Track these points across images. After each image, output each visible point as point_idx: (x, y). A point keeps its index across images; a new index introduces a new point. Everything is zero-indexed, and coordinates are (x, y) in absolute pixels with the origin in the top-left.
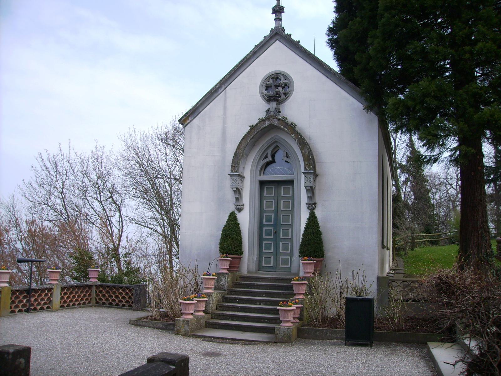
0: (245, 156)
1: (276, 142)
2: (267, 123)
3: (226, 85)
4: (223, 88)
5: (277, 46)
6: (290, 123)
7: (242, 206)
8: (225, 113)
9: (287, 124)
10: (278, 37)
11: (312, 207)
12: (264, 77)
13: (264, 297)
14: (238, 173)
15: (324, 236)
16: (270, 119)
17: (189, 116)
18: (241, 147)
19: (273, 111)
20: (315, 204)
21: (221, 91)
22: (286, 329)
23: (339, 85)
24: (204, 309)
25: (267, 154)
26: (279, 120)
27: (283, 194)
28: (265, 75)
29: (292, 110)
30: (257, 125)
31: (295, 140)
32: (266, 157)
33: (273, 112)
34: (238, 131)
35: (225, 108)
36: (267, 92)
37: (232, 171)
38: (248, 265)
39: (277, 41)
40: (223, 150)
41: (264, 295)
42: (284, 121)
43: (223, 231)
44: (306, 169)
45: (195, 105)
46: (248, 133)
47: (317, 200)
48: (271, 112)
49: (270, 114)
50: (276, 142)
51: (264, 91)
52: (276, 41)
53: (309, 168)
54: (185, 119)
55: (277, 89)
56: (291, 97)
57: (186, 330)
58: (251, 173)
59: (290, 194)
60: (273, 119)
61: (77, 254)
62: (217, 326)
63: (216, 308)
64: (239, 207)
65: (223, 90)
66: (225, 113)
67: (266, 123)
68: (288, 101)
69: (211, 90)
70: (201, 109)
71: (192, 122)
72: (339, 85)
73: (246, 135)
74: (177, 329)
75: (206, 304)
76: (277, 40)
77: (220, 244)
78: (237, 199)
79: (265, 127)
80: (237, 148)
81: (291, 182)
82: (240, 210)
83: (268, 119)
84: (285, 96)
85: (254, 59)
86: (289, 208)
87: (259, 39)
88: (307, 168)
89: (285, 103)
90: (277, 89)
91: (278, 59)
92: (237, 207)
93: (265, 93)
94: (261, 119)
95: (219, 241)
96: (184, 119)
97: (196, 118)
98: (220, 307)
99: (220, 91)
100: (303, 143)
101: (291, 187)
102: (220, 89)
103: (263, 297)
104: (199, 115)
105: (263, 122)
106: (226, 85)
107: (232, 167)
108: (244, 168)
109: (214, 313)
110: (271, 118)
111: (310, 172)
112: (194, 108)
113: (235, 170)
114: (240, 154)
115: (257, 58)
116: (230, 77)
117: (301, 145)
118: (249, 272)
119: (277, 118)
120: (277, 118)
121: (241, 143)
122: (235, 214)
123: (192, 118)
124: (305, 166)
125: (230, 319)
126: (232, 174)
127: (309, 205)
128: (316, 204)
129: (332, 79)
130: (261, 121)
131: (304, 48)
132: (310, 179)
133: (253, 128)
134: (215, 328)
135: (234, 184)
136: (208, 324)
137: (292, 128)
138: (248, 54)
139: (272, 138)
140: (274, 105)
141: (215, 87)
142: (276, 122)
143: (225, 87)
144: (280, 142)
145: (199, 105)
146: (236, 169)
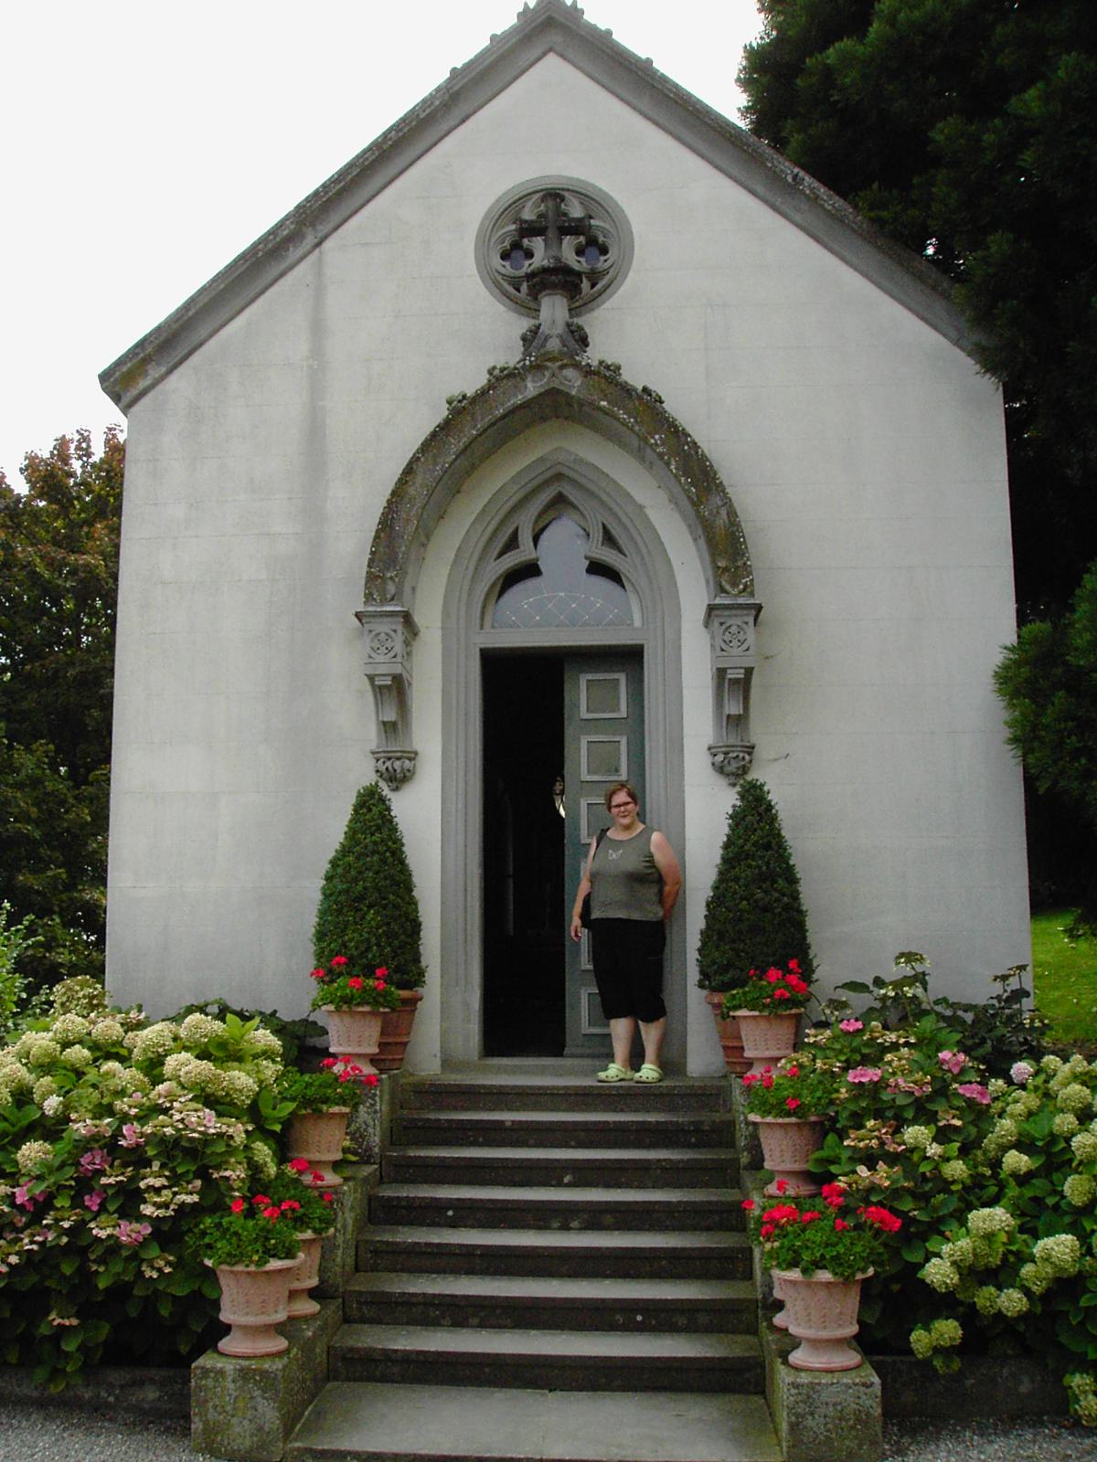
0: (423, 539)
1: (559, 477)
2: (532, 388)
3: (319, 227)
4: (310, 240)
5: (553, 74)
6: (641, 388)
7: (410, 759)
8: (317, 352)
9: (627, 390)
10: (556, 38)
11: (734, 762)
12: (505, 194)
13: (569, 1185)
14: (399, 609)
15: (809, 895)
16: (547, 368)
17: (147, 360)
18: (412, 491)
19: (560, 336)
20: (750, 749)
21: (300, 252)
22: (848, 1386)
23: (835, 247)
24: (314, 1282)
25: (517, 529)
26: (588, 372)
27: (588, 710)
28: (492, 200)
29: (635, 333)
30: (483, 394)
31: (668, 464)
32: (512, 543)
33: (557, 341)
34: (385, 428)
35: (318, 329)
36: (507, 264)
37: (369, 597)
38: (444, 1034)
39: (551, 54)
40: (313, 514)
41: (566, 1180)
42: (608, 376)
43: (329, 878)
44: (723, 590)
45: (178, 311)
46: (445, 428)
47: (758, 732)
48: (547, 338)
49: (543, 345)
50: (559, 477)
51: (497, 262)
52: (544, 54)
53: (734, 585)
54: (130, 372)
55: (556, 249)
56: (622, 289)
57: (260, 1429)
58: (446, 614)
59: (616, 708)
60: (562, 367)
61: (1021, 294)
62: (396, 1369)
63: (350, 1261)
64: (397, 764)
65: (310, 252)
66: (317, 352)
67: (530, 385)
68: (607, 305)
69: (254, 247)
70: (203, 333)
71: (160, 387)
72: (835, 247)
73: (434, 435)
74: (206, 1423)
75: (323, 1256)
76: (551, 50)
77: (321, 935)
78: (389, 729)
79: (526, 405)
80: (394, 493)
81: (629, 658)
82: (399, 779)
83: (537, 368)
84: (593, 286)
85: (452, 123)
86: (617, 770)
87: (467, 46)
88: (728, 587)
89: (595, 313)
90: (556, 249)
91: (555, 134)
92: (388, 764)
93: (503, 271)
94: (502, 370)
95: (310, 920)
96: (125, 369)
97: (181, 369)
98: (376, 1252)
99: (294, 254)
100: (696, 477)
101: (622, 677)
102: (296, 247)
103: (560, 1184)
104: (196, 359)
105: (511, 383)
106: (323, 229)
107: (371, 578)
108: (414, 589)
109: (360, 1293)
110: (549, 364)
111: (740, 601)
112: (177, 320)
113: (383, 592)
114: (408, 520)
115: (463, 121)
116: (339, 194)
117: (692, 484)
118: (447, 1063)
119: (577, 366)
120: (577, 366)
121: (409, 471)
122: (382, 800)
123: (163, 370)
124: (715, 576)
125: (447, 1321)
126: (371, 609)
127: (726, 753)
128: (753, 747)
129: (798, 218)
130: (502, 378)
131: (676, 86)
132: (741, 637)
133: (461, 409)
134: (385, 1379)
135: (381, 659)
136: (344, 1358)
137: (645, 420)
138: (424, 101)
139: (542, 460)
140: (554, 309)
141: (273, 232)
142: (573, 382)
143: (320, 235)
144: (576, 476)
145: (197, 313)
146: (391, 588)
